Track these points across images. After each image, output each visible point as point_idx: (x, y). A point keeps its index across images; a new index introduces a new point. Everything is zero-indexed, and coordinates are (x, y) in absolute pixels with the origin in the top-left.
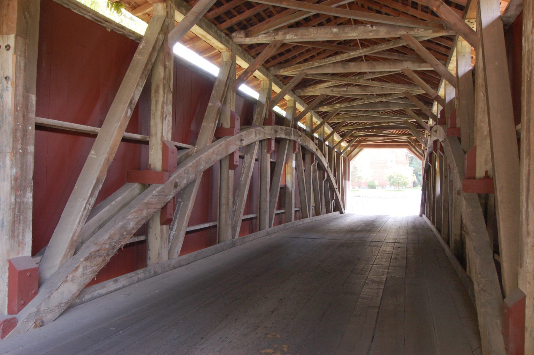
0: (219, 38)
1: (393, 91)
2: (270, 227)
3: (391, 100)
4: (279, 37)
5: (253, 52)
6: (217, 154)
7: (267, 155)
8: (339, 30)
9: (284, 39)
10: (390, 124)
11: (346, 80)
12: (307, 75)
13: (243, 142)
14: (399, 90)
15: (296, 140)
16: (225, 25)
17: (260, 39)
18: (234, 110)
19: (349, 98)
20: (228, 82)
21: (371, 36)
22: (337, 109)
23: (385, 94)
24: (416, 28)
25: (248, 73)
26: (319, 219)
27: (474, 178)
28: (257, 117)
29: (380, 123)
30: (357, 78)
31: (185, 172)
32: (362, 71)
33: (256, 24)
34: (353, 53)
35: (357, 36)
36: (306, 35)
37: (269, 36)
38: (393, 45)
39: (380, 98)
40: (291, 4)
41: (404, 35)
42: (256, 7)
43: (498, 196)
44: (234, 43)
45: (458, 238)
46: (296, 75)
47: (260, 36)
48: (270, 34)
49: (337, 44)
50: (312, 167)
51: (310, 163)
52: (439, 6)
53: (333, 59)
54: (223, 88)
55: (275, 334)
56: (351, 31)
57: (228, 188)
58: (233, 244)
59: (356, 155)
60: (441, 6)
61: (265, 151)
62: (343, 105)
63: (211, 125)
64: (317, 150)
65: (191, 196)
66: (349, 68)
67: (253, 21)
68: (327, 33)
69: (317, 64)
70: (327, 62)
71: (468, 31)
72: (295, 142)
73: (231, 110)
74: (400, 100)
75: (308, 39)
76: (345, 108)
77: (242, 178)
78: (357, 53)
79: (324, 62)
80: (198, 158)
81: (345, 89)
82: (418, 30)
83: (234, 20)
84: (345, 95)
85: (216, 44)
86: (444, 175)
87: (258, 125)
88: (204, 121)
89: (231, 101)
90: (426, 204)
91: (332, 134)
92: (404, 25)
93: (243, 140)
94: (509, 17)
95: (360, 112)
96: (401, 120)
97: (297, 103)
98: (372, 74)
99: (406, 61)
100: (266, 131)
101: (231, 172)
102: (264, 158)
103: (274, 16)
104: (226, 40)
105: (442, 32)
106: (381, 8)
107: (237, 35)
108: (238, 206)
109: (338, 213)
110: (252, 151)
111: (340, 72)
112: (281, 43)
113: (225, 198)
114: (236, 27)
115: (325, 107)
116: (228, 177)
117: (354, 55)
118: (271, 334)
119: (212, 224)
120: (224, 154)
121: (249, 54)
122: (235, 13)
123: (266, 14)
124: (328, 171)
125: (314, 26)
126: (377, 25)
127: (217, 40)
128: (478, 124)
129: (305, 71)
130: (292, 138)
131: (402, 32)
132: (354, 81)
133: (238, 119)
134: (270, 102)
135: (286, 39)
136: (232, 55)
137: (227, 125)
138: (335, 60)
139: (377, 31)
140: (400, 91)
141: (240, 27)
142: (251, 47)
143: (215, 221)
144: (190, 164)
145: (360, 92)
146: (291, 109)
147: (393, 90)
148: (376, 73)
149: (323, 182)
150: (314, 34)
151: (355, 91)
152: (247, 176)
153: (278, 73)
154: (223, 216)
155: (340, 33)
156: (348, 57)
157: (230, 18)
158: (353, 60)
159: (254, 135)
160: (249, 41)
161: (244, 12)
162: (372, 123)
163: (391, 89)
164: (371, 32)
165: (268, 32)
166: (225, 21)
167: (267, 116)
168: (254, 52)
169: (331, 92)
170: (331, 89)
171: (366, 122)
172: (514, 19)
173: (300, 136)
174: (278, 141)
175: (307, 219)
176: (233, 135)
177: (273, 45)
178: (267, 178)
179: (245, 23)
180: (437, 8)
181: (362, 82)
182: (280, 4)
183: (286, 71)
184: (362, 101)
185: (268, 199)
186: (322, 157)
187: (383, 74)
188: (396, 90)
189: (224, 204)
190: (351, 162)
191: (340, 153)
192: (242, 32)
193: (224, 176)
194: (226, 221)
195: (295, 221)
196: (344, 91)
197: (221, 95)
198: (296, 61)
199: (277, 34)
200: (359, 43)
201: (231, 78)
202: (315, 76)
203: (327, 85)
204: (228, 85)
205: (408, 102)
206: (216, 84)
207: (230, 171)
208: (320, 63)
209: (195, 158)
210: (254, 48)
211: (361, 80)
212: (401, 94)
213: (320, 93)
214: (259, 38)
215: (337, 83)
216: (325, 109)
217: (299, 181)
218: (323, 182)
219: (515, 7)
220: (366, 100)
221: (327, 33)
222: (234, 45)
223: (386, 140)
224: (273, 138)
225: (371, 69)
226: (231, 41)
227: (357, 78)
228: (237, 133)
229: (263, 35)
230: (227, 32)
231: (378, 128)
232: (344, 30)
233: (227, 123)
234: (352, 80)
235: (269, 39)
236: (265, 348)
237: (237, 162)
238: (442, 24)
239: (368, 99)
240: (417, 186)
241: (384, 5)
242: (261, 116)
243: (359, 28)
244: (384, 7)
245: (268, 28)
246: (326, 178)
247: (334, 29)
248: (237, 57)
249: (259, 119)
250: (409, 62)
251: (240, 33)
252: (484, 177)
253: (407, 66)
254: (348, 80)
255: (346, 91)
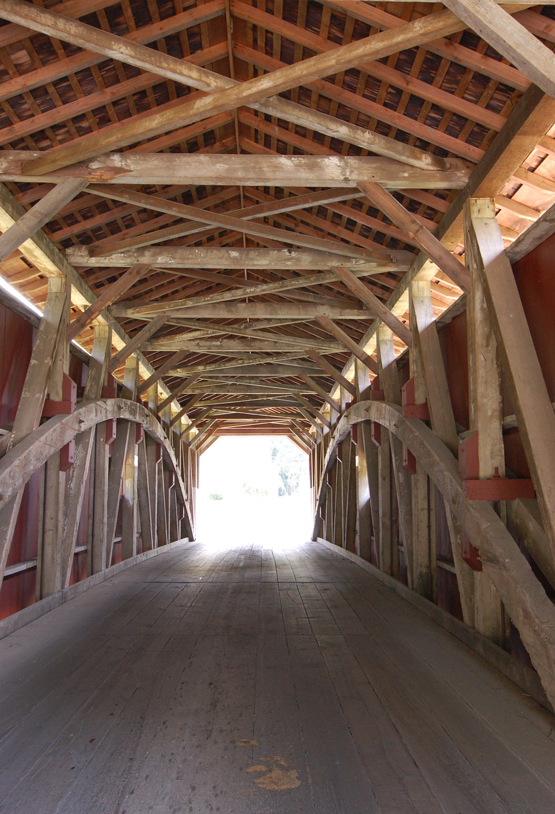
0: (51, 255)
1: (291, 348)
2: (107, 567)
3: (282, 361)
4: (146, 259)
5: (92, 279)
6: (50, 445)
7: (105, 446)
8: (241, 254)
9: (153, 263)
10: (270, 398)
11: (227, 329)
12: (169, 319)
13: (82, 424)
14: (299, 347)
15: (141, 422)
16: (60, 235)
17: (114, 261)
18: (67, 372)
19: (224, 358)
20: (61, 327)
21: (290, 266)
22: (197, 375)
23: (267, 352)
24: (353, 258)
25: (93, 313)
26: (165, 551)
27: (477, 478)
28: (91, 385)
29: (256, 397)
30: (242, 327)
31: (10, 476)
32: (256, 317)
33: (106, 237)
34: (252, 290)
35: (267, 265)
36: (188, 259)
37: (130, 256)
38: (315, 281)
39: (268, 359)
40: (184, 211)
41: (337, 268)
42: (112, 211)
43: (548, 504)
44: (70, 264)
45: (424, 570)
46: (152, 318)
47: (113, 256)
48: (131, 253)
49: (218, 273)
50: (157, 464)
51: (155, 459)
52: (418, 231)
53: (218, 297)
54: (55, 336)
55: (247, 740)
56: (258, 258)
57: (57, 503)
58: (64, 599)
59: (208, 446)
60: (421, 231)
61: (102, 440)
62: (209, 368)
63: (37, 395)
64: (165, 438)
65: (11, 516)
66: (237, 312)
67: (102, 232)
68: (222, 257)
69: (191, 303)
70: (208, 300)
71: (457, 268)
72: (139, 425)
73: (64, 373)
74: (295, 362)
75: (191, 264)
76: (211, 372)
77: (71, 484)
78: (258, 290)
79: (204, 301)
80: (27, 451)
81: (218, 343)
82: (356, 262)
83: (77, 229)
84: (218, 352)
85: (45, 263)
86: (382, 476)
87: (94, 397)
88: (24, 390)
89: (63, 357)
90: (325, 523)
91: (180, 415)
92: (340, 253)
93: (83, 422)
94: (518, 253)
95: (231, 379)
96: (290, 392)
97: (140, 363)
98: (266, 322)
99: (322, 305)
100: (108, 408)
101: (62, 474)
102: (99, 451)
103: (136, 225)
104: (60, 258)
105: (391, 266)
106: (297, 225)
107: (75, 251)
108: (66, 533)
109: (186, 540)
110: (87, 440)
111: (223, 317)
112: (148, 269)
113: (52, 519)
114: (75, 240)
115: (179, 370)
116: (58, 484)
117: (253, 292)
118: (241, 740)
119: (30, 565)
120: (59, 444)
121: (86, 282)
122: (80, 218)
123: (124, 222)
124: (177, 472)
125: (189, 246)
126: (298, 251)
127: (49, 258)
128: (479, 399)
129: (167, 314)
130: (138, 419)
131: (334, 263)
132: (238, 331)
133: (74, 388)
134: (109, 360)
135: (157, 264)
136: (66, 283)
137: (57, 397)
138: (223, 298)
139: (298, 260)
140: (301, 349)
141: (80, 239)
142: (90, 272)
143: (33, 558)
144: (17, 462)
145: (242, 348)
146: (131, 374)
147: (292, 347)
148: (273, 320)
149: (170, 490)
150: (201, 257)
151: (234, 347)
152: (80, 481)
153: (123, 315)
154: (48, 550)
155: (242, 259)
156: (244, 295)
157: (69, 225)
158: (252, 300)
159: (95, 414)
160: (94, 262)
161: (93, 216)
162: (244, 397)
163: (288, 345)
164: (289, 260)
165: (129, 251)
166: (61, 229)
167: (106, 384)
168: (93, 279)
169: (197, 348)
170: (196, 342)
171: (235, 394)
172: (523, 256)
173: (147, 416)
174: (121, 422)
175: (151, 551)
176: (69, 413)
177: (135, 271)
178: (104, 485)
179: (90, 234)
180: (415, 234)
181: (249, 333)
182: (168, 209)
183: (138, 312)
184: (240, 362)
185: (106, 520)
186: (170, 449)
187: (285, 322)
188: (296, 348)
189: (50, 530)
190: (201, 457)
191: (187, 443)
192: (84, 247)
193: (51, 482)
194: (53, 558)
195: (138, 555)
196: (216, 346)
197: (52, 347)
198: (150, 297)
199: (142, 255)
200: (246, 275)
201: (64, 320)
202: (180, 321)
203: (193, 336)
204: (60, 330)
205: (306, 365)
206: (42, 328)
207: (61, 472)
208: (196, 303)
209: (23, 452)
210: (94, 273)
211: (249, 331)
212: (301, 354)
213: (178, 348)
214: (112, 259)
215: (211, 332)
216: (180, 373)
217: (141, 489)
218: (170, 490)
219: (531, 240)
220: (246, 361)
221: (222, 257)
222: (69, 267)
223: (257, 423)
224: (115, 419)
225: (271, 314)
226: (65, 261)
227: (242, 327)
228: (75, 410)
229: (119, 255)
230: (61, 247)
231: (251, 404)
232: (247, 255)
233: (57, 393)
234: (235, 330)
235: (129, 261)
236: (248, 764)
237: (72, 458)
238: (390, 256)
239: (250, 360)
240: (284, 494)
241: (302, 222)
242: (99, 384)
243: (271, 252)
244: (301, 225)
245: (131, 245)
246: (174, 484)
247: (233, 252)
248: (72, 288)
249: (96, 387)
250: (325, 307)
251: (80, 249)
252: (494, 477)
253: (323, 313)
254: (230, 330)
255: (220, 347)
